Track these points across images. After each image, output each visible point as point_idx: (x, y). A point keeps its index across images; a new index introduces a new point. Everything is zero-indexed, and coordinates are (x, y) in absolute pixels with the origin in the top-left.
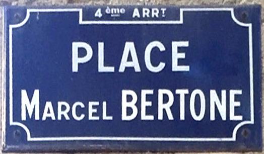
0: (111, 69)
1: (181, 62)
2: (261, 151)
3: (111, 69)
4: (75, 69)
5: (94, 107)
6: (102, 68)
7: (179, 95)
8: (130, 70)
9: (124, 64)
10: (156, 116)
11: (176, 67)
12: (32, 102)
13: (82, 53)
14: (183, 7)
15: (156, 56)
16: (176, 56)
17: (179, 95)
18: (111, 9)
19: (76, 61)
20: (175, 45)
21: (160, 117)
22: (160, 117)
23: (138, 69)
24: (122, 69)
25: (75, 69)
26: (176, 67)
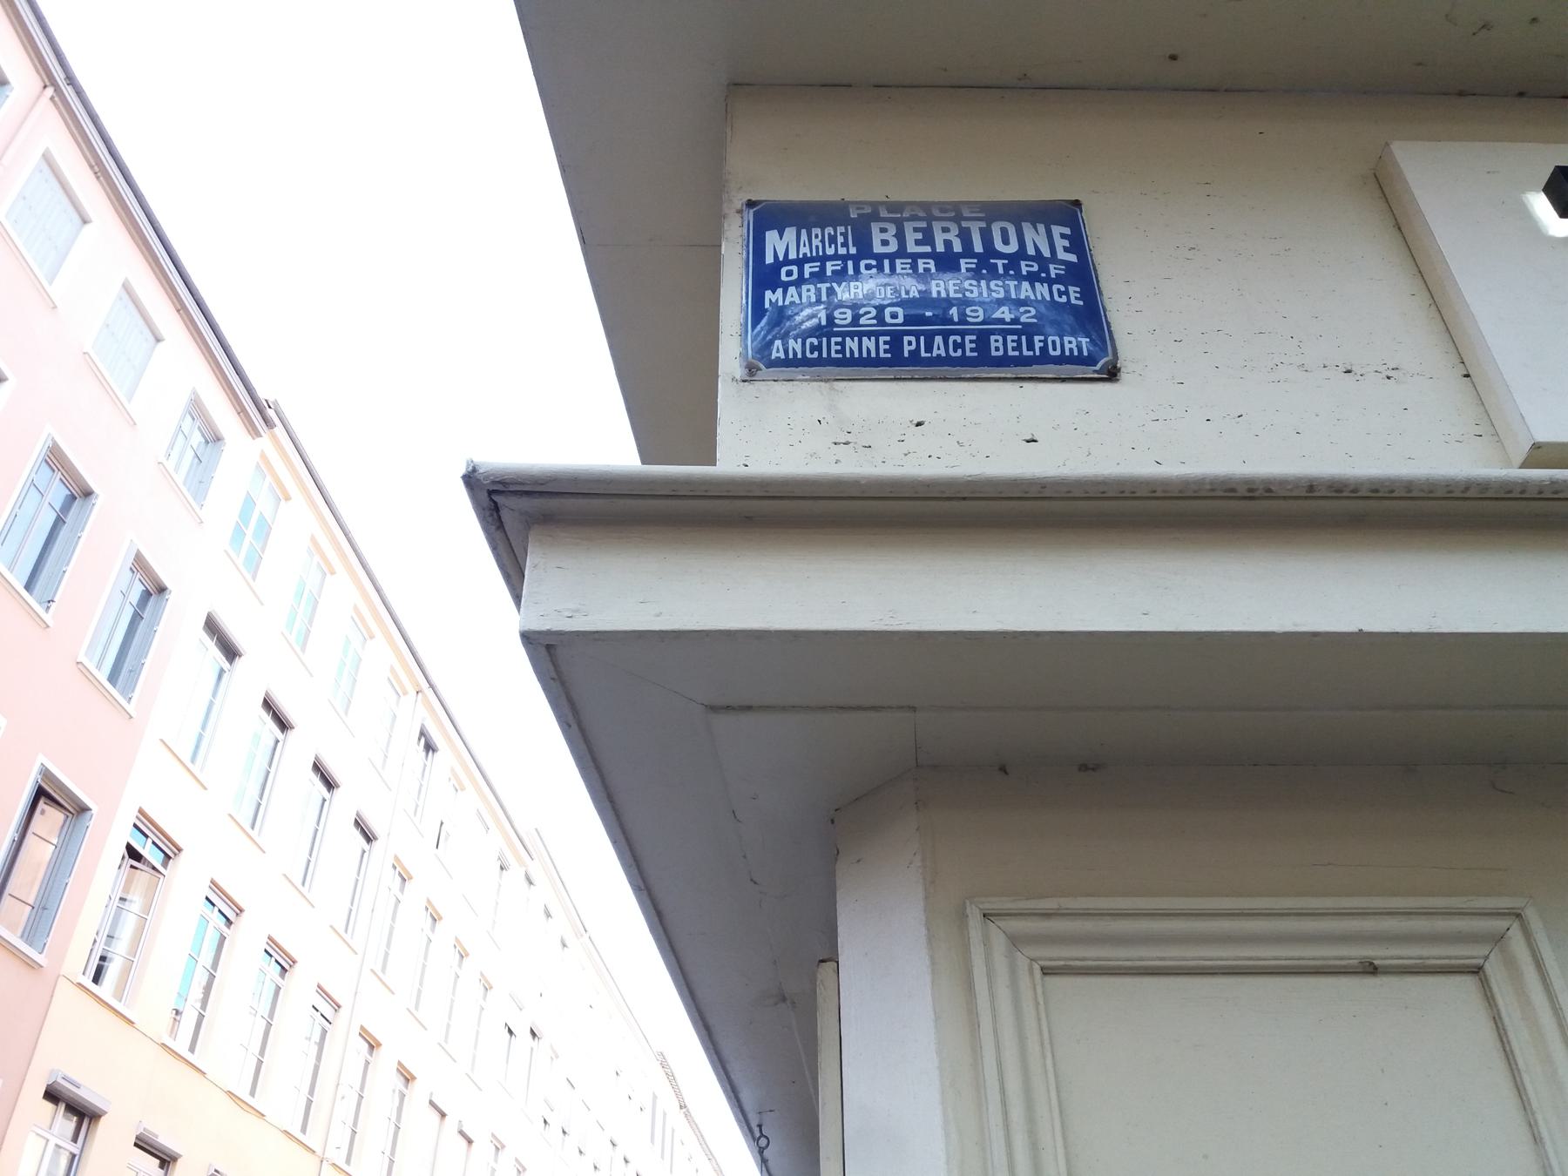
0: (929, 355)
1: (972, 350)
2: (338, 786)
3: (929, 355)
4: (906, 354)
5: (836, 344)
6: (923, 354)
7: (820, 288)
8: (939, 356)
9: (935, 352)
10: (844, 354)
11: (968, 353)
12: (783, 239)
13: (910, 343)
14: (889, 305)
15: (956, 346)
16: (968, 346)
17: (820, 288)
18: (875, 307)
19: (907, 349)
20: (968, 338)
21: (848, 355)
22: (848, 355)
23: (944, 354)
24: (934, 355)
25: (906, 354)
26: (968, 353)
